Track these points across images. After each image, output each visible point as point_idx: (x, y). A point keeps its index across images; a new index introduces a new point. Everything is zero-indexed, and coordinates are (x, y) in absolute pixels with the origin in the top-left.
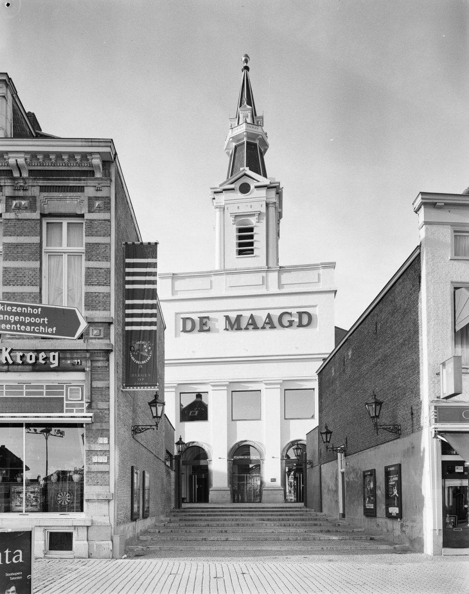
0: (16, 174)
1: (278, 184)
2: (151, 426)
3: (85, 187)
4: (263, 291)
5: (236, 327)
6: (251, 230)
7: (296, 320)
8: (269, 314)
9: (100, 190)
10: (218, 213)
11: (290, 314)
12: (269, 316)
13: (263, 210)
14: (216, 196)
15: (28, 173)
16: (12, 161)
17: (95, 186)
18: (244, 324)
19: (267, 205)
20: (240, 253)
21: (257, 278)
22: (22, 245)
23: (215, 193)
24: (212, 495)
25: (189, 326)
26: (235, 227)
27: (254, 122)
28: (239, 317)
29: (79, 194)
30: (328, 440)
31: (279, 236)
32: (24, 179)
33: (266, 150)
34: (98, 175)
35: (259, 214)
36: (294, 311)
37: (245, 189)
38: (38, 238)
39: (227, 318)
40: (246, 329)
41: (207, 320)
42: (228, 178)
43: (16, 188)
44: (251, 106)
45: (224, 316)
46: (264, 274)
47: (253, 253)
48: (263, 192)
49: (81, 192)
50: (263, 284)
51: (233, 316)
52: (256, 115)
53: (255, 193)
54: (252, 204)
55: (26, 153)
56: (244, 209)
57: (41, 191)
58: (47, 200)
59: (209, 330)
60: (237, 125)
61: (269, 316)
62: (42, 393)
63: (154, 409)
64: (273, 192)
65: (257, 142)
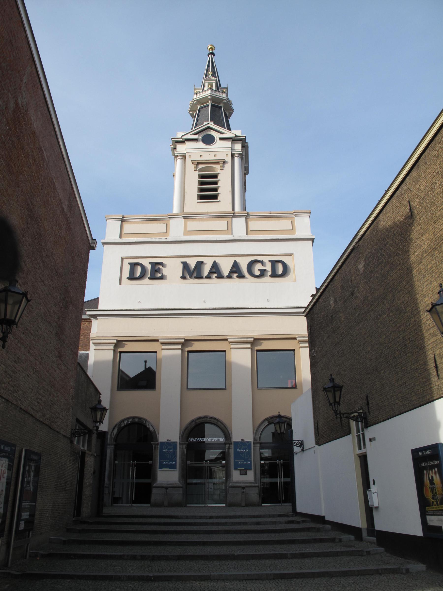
1: (244, 138)
5: (195, 275)
6: (216, 176)
7: (269, 267)
10: (179, 162)
11: (261, 262)
13: (229, 159)
18: (206, 270)
19: (233, 156)
20: (201, 197)
21: (222, 224)
25: (139, 270)
26: (197, 173)
28: (200, 265)
30: (337, 400)
33: (231, 114)
36: (266, 259)
37: (209, 140)
39: (185, 266)
40: (209, 277)
41: (161, 267)
42: (192, 129)
44: (216, 78)
45: (181, 262)
47: (217, 198)
48: (228, 144)
51: (192, 263)
52: (220, 86)
53: (218, 144)
56: (206, 157)
59: (162, 278)
60: (202, 91)
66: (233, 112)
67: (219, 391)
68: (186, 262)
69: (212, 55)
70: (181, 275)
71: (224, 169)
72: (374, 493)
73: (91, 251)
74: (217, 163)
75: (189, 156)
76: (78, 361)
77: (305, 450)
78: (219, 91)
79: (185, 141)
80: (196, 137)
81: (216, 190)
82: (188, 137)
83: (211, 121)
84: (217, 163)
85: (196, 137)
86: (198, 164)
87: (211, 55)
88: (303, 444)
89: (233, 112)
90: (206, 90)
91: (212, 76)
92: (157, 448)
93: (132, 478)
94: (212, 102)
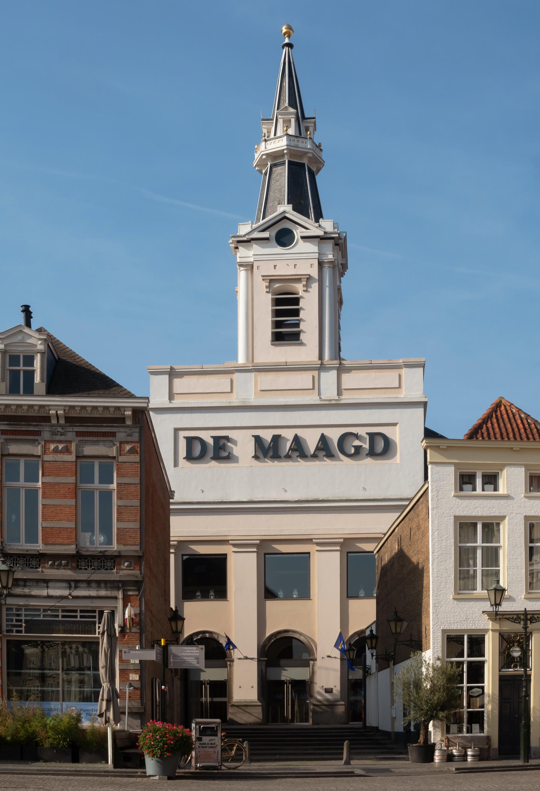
0: (54, 421)
2: (171, 641)
3: (117, 433)
4: (312, 399)
5: (271, 453)
7: (366, 446)
8: (323, 435)
9: (130, 436)
10: (242, 274)
11: (356, 436)
12: (323, 438)
13: (314, 273)
14: (239, 245)
15: (64, 420)
16: (52, 412)
17: (126, 432)
19: (321, 264)
22: (58, 484)
23: (239, 242)
24: (83, 533)
26: (270, 296)
27: (300, 134)
28: (276, 439)
29: (111, 438)
31: (341, 302)
32: (60, 426)
33: (319, 170)
34: (129, 422)
35: (308, 279)
36: (362, 432)
38: (74, 478)
39: (258, 440)
41: (224, 441)
43: (54, 433)
44: (297, 109)
45: (253, 436)
46: (316, 373)
48: (312, 248)
49: (113, 437)
50: (313, 388)
51: (267, 436)
52: (304, 118)
54: (296, 262)
55: (65, 406)
57: (77, 436)
58: (81, 444)
61: (323, 438)
62: (76, 617)
63: (173, 624)
64: (329, 247)
65: (305, 161)
66: (323, 166)
67: (220, 394)
68: (259, 436)
69: (290, 49)
70: (253, 454)
71: (309, 289)
72: (393, 709)
73: (31, 319)
74: (298, 280)
75: (258, 267)
76: (171, 607)
77: (373, 673)
78: (302, 136)
79: (251, 241)
80: (266, 235)
81: (296, 313)
82: (256, 235)
83: (288, 203)
84: (298, 280)
85: (266, 235)
86: (271, 281)
87: (287, 48)
88: (370, 669)
89: (324, 165)
90: (280, 137)
91: (289, 105)
92: (232, 665)
93: (205, 697)
94: (290, 159)
